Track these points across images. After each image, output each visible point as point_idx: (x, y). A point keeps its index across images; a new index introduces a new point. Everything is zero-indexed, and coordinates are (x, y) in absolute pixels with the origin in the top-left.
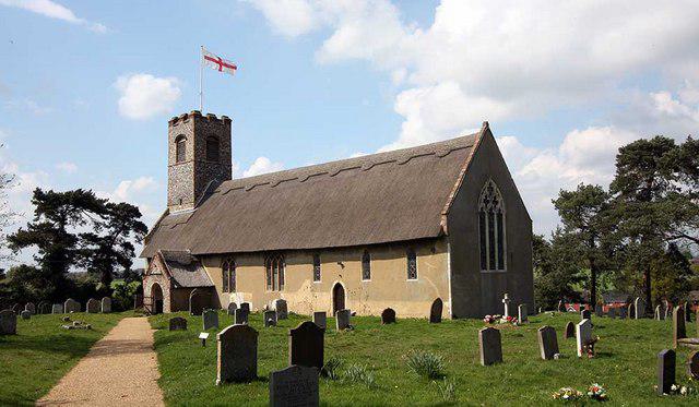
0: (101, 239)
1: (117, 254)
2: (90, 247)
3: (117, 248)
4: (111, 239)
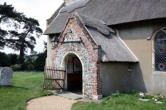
0: (20, 34)
1: (27, 42)
2: (14, 38)
3: (27, 39)
4: (24, 35)
